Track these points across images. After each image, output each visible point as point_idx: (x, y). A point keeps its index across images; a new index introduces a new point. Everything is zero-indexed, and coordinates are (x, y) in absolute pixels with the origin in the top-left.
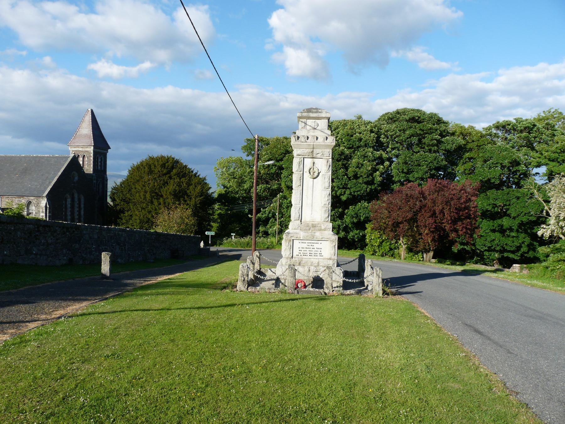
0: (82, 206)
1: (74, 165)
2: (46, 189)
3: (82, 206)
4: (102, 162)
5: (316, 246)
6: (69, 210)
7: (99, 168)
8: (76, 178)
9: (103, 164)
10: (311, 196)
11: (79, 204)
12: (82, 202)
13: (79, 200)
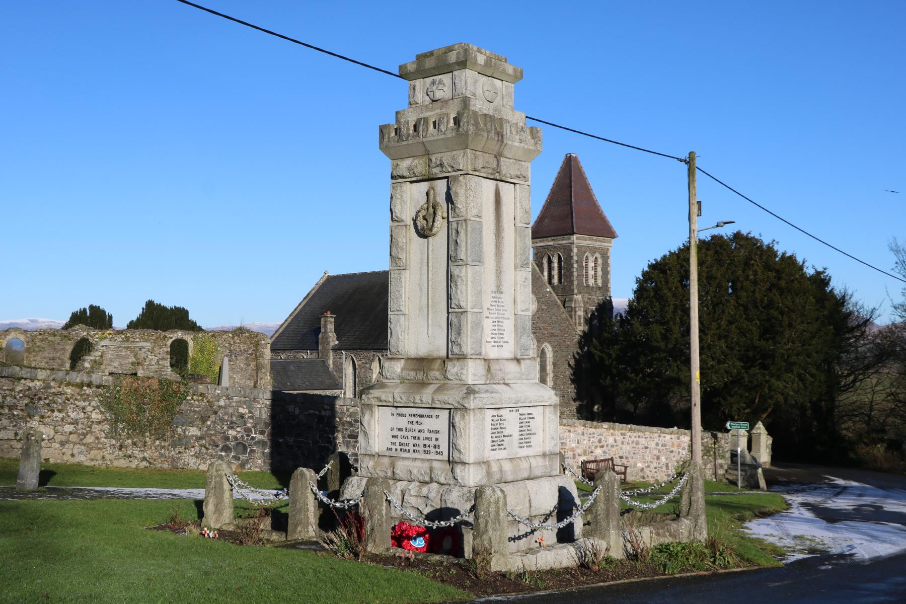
4: (599, 269)
7: (591, 282)
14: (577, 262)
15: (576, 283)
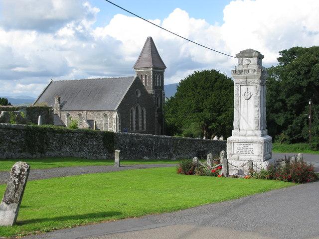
0: (145, 117)
1: (137, 83)
2: (117, 104)
3: (145, 117)
4: (160, 80)
5: (249, 147)
6: (134, 120)
7: (158, 84)
8: (139, 95)
9: (160, 81)
10: (248, 112)
11: (142, 115)
12: (145, 112)
13: (142, 112)
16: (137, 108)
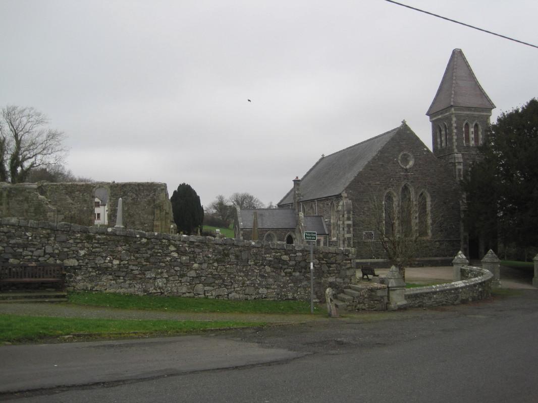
7: (472, 143)
14: (456, 128)
15: (455, 144)
16: (406, 188)
